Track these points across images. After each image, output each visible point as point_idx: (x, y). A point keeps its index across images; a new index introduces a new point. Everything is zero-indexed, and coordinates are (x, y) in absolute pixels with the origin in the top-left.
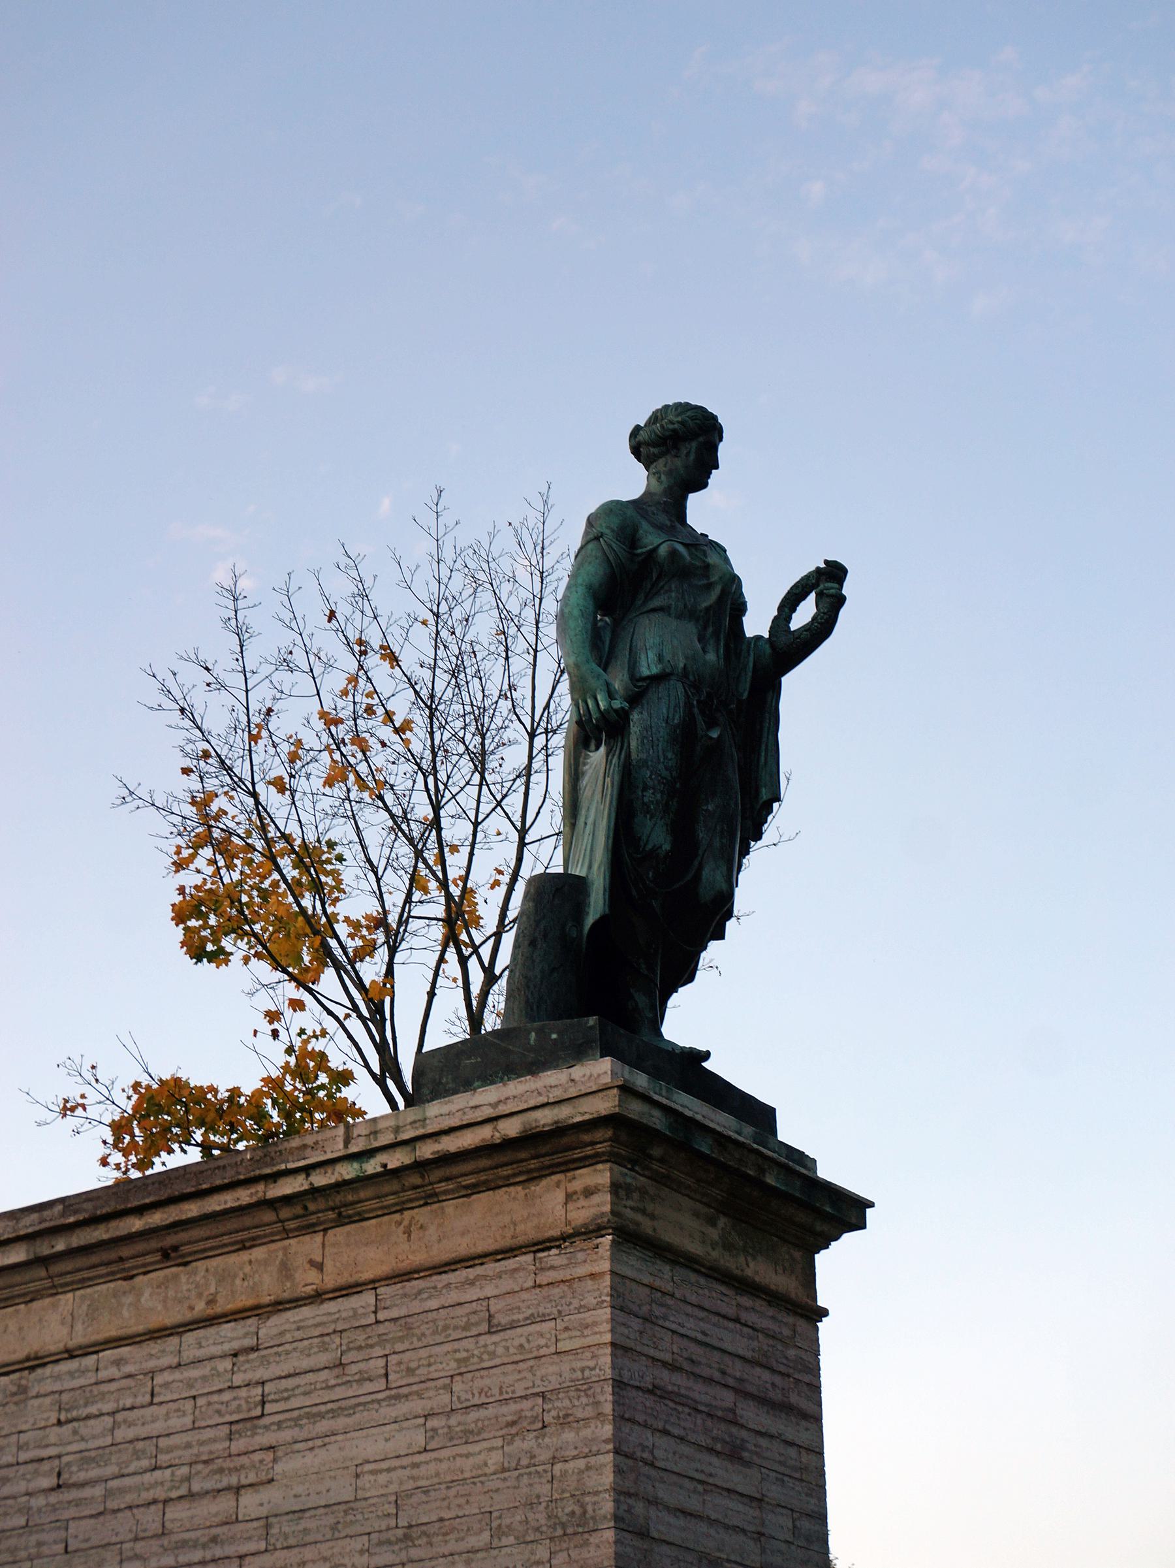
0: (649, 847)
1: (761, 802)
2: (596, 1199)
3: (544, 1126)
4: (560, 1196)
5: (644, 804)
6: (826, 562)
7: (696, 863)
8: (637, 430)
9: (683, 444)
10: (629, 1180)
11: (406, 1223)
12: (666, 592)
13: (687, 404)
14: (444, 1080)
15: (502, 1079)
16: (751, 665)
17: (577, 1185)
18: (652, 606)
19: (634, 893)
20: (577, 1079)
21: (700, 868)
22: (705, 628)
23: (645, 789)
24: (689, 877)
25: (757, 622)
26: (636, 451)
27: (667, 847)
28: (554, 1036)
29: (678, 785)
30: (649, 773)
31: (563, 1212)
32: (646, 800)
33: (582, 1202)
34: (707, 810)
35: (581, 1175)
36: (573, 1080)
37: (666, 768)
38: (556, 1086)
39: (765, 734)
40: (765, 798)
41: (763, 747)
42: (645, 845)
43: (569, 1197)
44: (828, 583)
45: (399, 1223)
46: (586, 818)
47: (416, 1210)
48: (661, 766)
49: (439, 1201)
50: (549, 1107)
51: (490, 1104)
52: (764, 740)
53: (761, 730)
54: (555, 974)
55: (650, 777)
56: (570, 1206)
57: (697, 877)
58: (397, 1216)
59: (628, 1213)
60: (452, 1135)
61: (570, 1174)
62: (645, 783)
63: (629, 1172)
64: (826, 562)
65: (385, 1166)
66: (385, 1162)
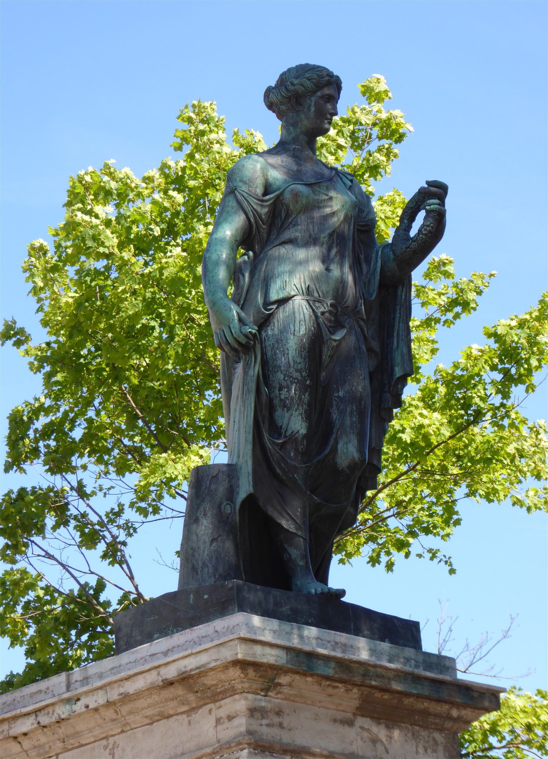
0: (289, 432)
1: (395, 378)
2: (236, 722)
3: (191, 670)
4: (212, 720)
5: (281, 400)
6: (427, 183)
7: (332, 441)
8: (269, 91)
9: (306, 99)
10: (263, 704)
11: (111, 746)
12: (294, 225)
13: (307, 65)
14: (134, 634)
15: (172, 631)
16: (379, 270)
17: (223, 713)
18: (282, 240)
19: (278, 470)
20: (219, 630)
21: (336, 443)
22: (329, 249)
23: (280, 389)
24: (327, 452)
25: (387, 231)
26: (270, 106)
27: (303, 431)
28: (206, 597)
29: (308, 382)
30: (282, 377)
31: (215, 732)
32: (283, 397)
33: (227, 724)
34: (338, 397)
35: (225, 704)
36: (216, 631)
37: (297, 371)
38: (205, 637)
39: (397, 323)
40: (398, 375)
41: (395, 334)
42: (286, 432)
43: (218, 721)
44: (432, 196)
45: (105, 748)
46: (235, 418)
47: (117, 737)
48: (292, 370)
49: (132, 729)
50: (193, 656)
51: (162, 653)
52: (396, 328)
53: (394, 319)
54: (214, 544)
55: (284, 379)
56: (219, 727)
57: (335, 449)
58: (104, 742)
59: (265, 730)
60: (130, 680)
61: (218, 704)
62: (280, 384)
63: (263, 698)
64: (427, 183)
65: (87, 707)
66: (87, 703)
